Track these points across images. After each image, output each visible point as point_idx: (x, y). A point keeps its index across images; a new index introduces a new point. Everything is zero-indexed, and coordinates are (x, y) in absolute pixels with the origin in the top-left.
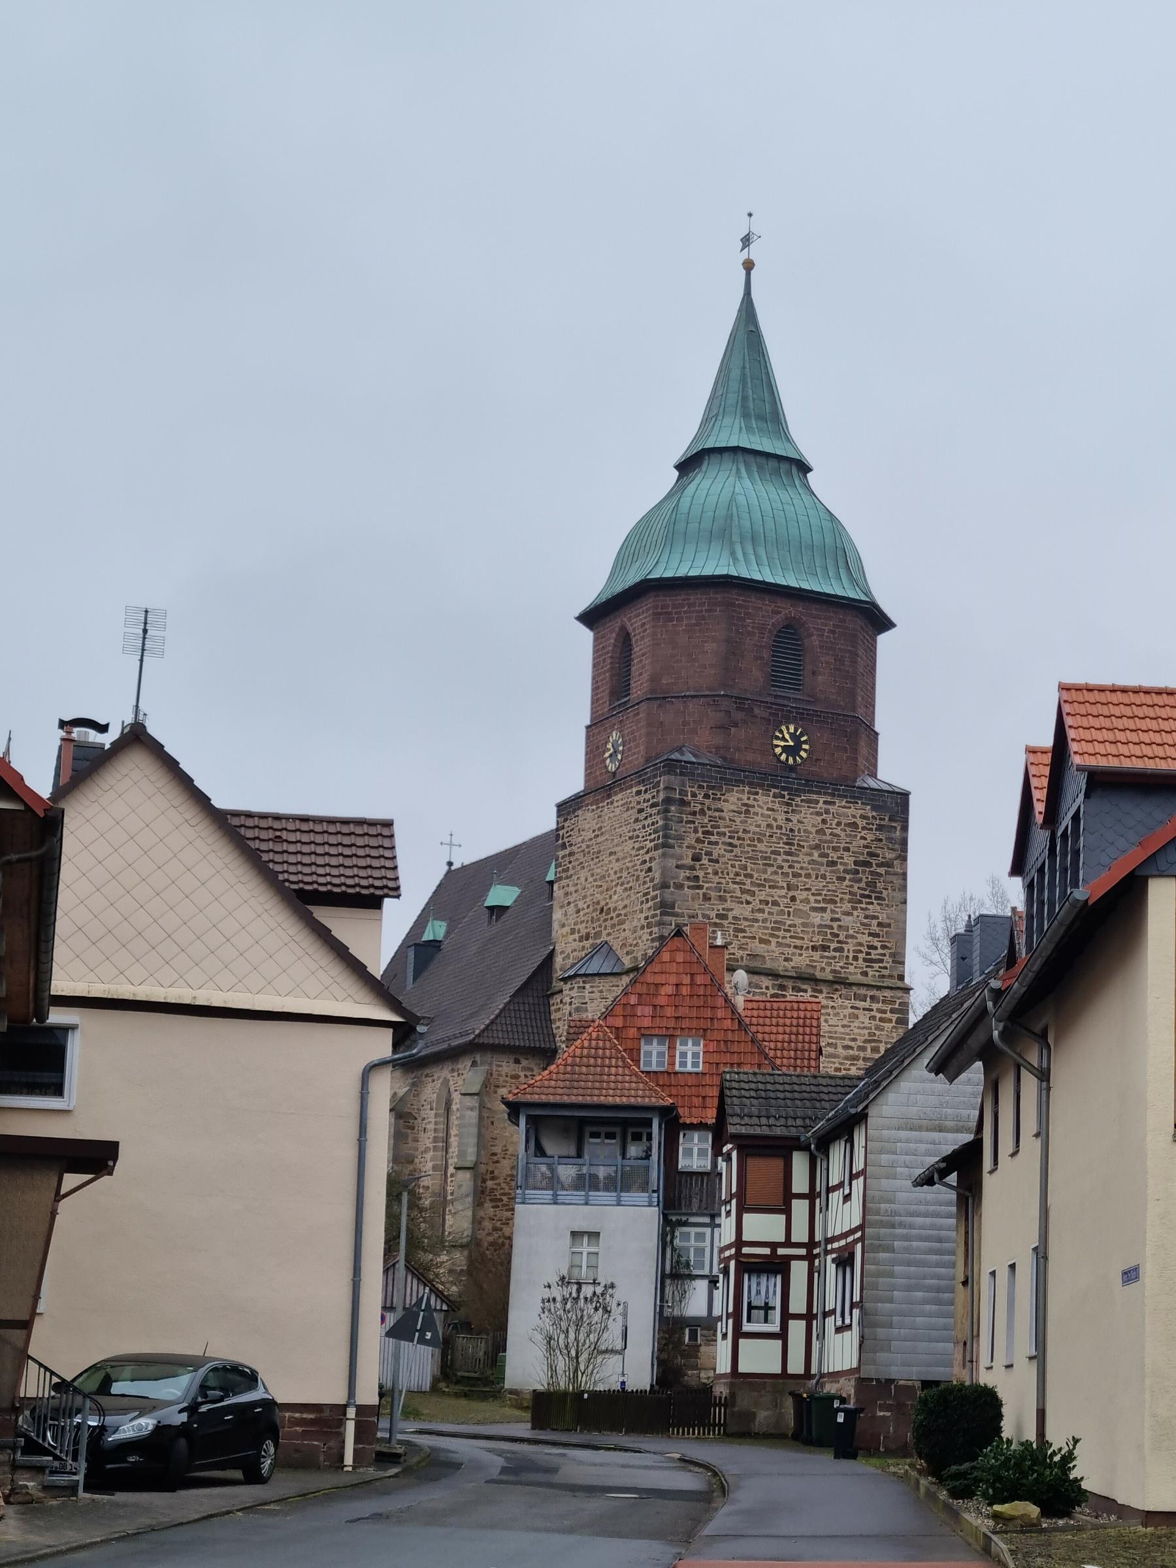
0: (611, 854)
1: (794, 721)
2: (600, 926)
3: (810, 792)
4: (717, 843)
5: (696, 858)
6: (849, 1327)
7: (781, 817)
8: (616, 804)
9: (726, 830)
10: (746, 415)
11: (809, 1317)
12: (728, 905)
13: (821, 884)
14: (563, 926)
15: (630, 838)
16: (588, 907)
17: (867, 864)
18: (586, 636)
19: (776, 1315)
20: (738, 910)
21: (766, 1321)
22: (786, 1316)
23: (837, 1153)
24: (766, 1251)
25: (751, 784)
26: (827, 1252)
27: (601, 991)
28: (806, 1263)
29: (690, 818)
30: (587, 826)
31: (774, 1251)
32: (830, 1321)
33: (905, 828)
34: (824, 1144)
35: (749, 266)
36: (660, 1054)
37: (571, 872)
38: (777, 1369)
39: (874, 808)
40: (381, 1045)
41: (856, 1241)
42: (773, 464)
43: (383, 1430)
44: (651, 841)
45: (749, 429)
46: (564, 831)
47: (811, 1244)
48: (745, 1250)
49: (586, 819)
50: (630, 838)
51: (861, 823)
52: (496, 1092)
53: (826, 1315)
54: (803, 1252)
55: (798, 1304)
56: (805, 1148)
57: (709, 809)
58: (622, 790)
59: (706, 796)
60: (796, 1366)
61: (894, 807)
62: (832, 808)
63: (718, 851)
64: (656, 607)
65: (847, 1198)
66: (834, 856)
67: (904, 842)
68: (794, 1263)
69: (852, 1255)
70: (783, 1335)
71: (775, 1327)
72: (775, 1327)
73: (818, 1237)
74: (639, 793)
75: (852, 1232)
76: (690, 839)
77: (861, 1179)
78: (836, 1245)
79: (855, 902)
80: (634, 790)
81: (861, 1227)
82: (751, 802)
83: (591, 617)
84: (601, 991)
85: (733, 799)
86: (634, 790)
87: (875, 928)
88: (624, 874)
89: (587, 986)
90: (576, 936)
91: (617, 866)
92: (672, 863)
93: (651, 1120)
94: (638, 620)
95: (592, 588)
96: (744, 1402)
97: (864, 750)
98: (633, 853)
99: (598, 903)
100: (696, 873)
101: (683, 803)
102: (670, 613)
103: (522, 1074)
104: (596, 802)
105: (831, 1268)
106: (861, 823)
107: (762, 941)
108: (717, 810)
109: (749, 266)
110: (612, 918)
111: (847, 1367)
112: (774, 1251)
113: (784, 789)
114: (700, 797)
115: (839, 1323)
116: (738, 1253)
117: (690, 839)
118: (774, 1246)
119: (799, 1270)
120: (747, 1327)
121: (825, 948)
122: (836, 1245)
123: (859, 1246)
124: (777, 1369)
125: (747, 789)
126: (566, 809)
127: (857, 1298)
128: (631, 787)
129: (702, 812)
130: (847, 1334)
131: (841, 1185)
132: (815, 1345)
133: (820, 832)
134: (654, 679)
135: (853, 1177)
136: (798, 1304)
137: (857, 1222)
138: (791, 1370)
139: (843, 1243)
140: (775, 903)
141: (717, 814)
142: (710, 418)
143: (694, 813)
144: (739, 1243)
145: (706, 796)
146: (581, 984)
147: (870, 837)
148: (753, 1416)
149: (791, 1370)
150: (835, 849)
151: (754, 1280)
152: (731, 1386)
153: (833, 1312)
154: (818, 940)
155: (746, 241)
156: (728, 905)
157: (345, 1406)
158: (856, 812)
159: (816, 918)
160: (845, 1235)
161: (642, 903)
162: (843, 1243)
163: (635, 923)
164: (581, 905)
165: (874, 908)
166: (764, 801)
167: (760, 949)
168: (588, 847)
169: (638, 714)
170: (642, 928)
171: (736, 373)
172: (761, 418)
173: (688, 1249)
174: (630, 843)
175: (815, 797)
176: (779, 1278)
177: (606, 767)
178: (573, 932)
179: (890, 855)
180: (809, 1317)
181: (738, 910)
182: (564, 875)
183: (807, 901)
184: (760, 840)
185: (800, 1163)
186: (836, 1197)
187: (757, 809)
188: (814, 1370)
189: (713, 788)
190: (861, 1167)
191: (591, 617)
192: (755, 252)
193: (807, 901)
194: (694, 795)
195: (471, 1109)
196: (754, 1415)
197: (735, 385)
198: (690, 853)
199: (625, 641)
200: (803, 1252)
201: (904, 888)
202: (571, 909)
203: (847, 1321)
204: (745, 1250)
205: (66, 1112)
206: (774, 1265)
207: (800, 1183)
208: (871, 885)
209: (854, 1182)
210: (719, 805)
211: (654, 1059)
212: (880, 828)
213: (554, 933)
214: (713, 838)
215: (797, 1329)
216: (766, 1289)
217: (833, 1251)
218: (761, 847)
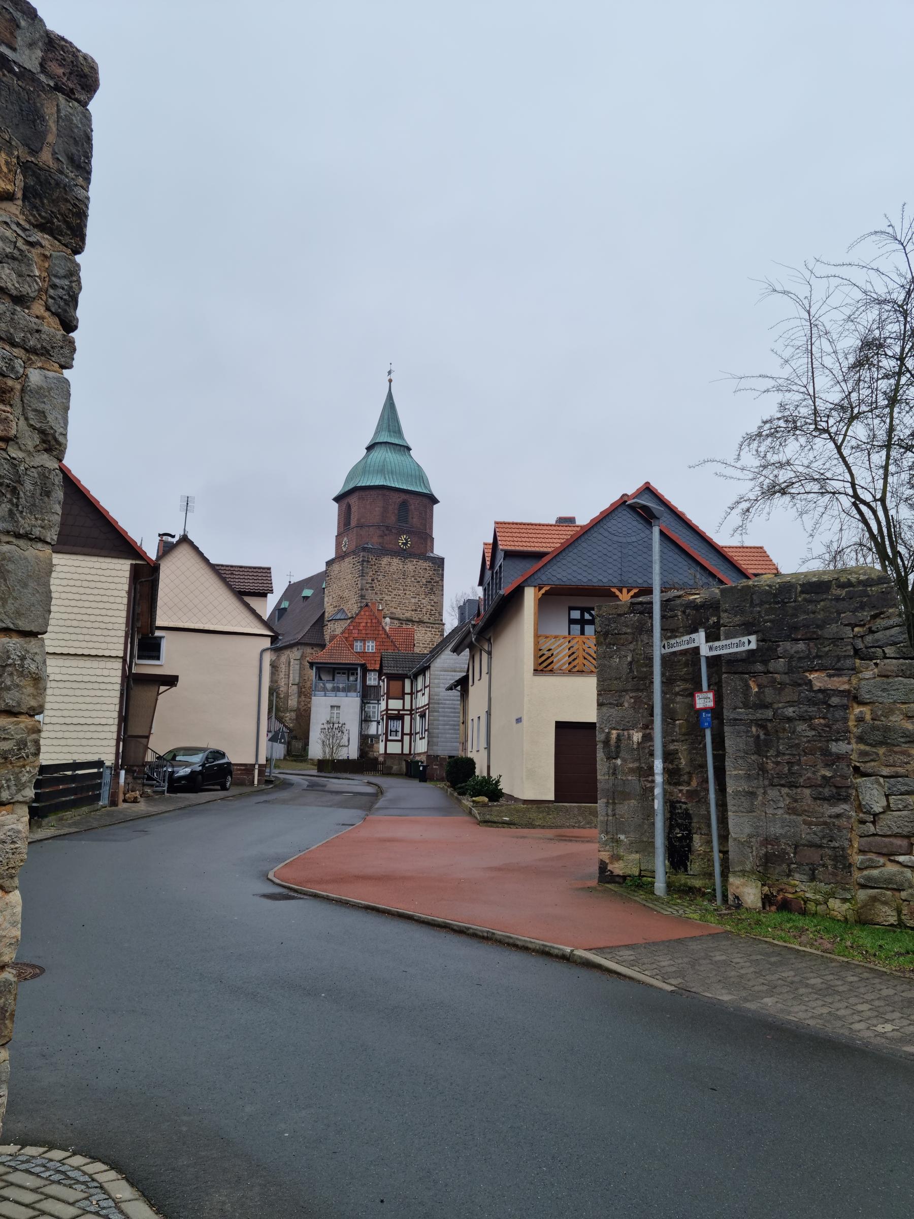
5: (373, 580)
10: (389, 431)
11: (410, 734)
20: (387, 598)
22: (403, 734)
23: (420, 679)
32: (418, 736)
34: (416, 676)
35: (390, 381)
40: (267, 643)
42: (398, 447)
45: (390, 436)
47: (411, 710)
49: (336, 567)
55: (407, 730)
60: (406, 751)
61: (439, 563)
65: (423, 694)
66: (419, 579)
67: (443, 575)
70: (402, 741)
71: (399, 738)
72: (399, 738)
76: (371, 574)
79: (426, 595)
81: (428, 704)
83: (337, 499)
85: (385, 560)
92: (364, 582)
94: (353, 500)
95: (338, 489)
96: (389, 763)
101: (368, 562)
105: (418, 718)
109: (390, 381)
117: (371, 574)
118: (399, 710)
119: (407, 719)
120: (390, 738)
126: (329, 563)
134: (358, 520)
135: (425, 687)
136: (407, 730)
137: (427, 702)
142: (377, 432)
144: (387, 709)
154: (414, 608)
155: (390, 373)
158: (426, 565)
159: (413, 600)
166: (396, 561)
171: (386, 417)
172: (394, 432)
180: (410, 734)
181: (387, 598)
185: (407, 683)
186: (420, 694)
191: (337, 499)
192: (392, 376)
197: (386, 421)
199: (349, 507)
201: (442, 590)
206: (399, 717)
207: (408, 689)
208: (432, 589)
215: (407, 738)
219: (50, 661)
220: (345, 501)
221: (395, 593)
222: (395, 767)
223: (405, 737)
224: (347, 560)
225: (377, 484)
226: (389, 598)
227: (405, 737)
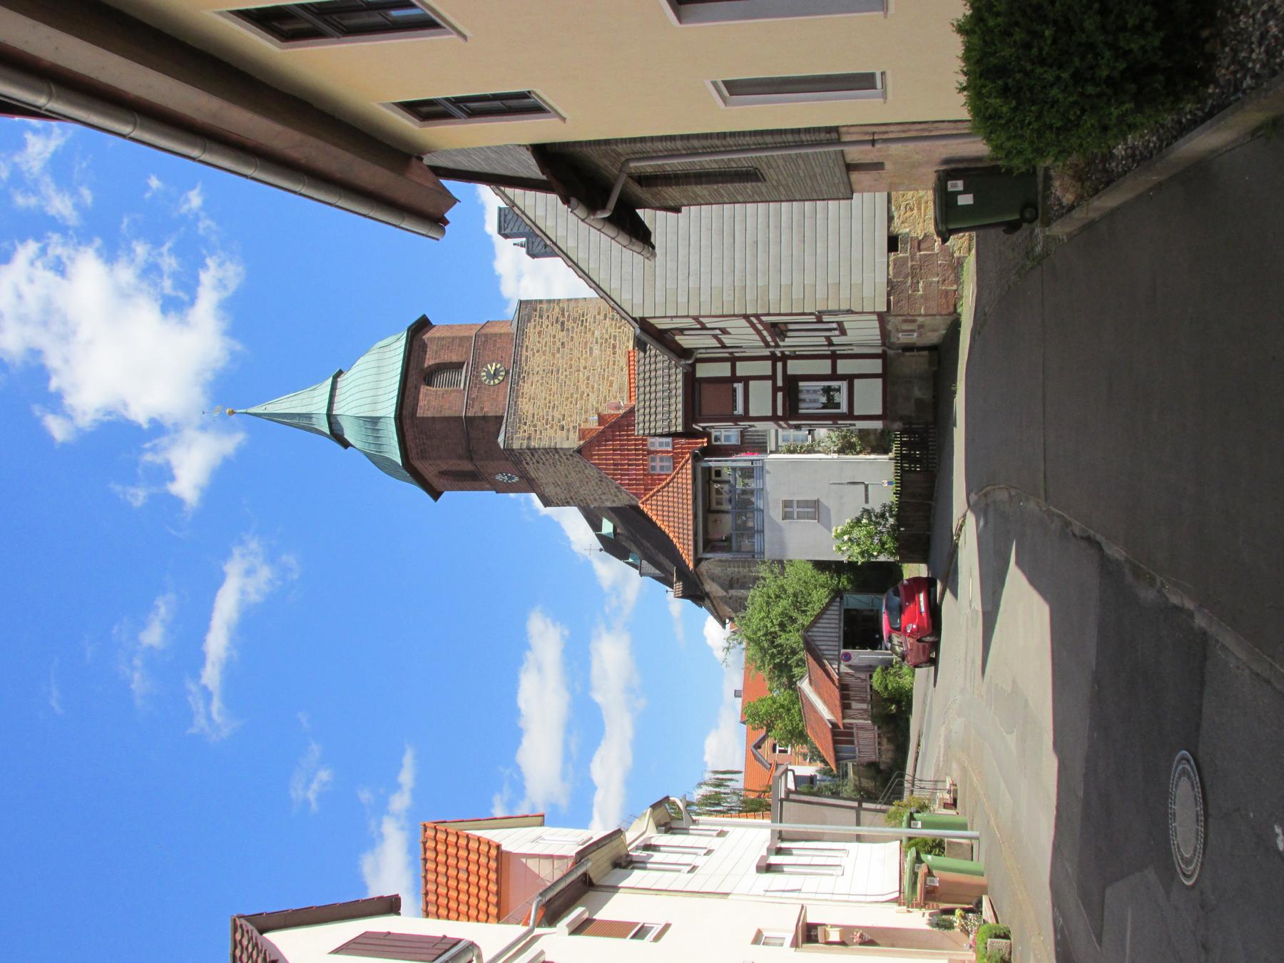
6: (840, 324)
11: (834, 357)
12: (590, 407)
13: (575, 352)
17: (563, 324)
18: (446, 494)
19: (834, 384)
21: (858, 824)
22: (834, 376)
23: (685, 341)
24: (780, 395)
26: (777, 346)
28: (790, 362)
31: (780, 389)
32: (835, 340)
33: (541, 301)
34: (683, 353)
36: (662, 460)
38: (879, 381)
39: (529, 321)
41: (761, 322)
47: (773, 358)
48: (780, 413)
49: (550, 491)
51: (538, 328)
53: (831, 344)
54: (779, 365)
55: (824, 367)
56: (693, 366)
60: (876, 366)
62: (531, 347)
63: (557, 415)
65: (724, 331)
67: (549, 301)
68: (790, 372)
69: (774, 325)
70: (850, 379)
71: (844, 385)
72: (844, 385)
73: (767, 352)
75: (753, 326)
78: (769, 339)
81: (746, 317)
83: (436, 495)
87: (602, 317)
91: (573, 474)
93: (703, 469)
94: (428, 469)
96: (908, 409)
97: (496, 330)
105: (788, 341)
106: (538, 328)
107: (611, 385)
111: (876, 324)
112: (780, 389)
115: (837, 333)
116: (784, 418)
117: (551, 432)
118: (775, 390)
119: (795, 367)
120: (844, 408)
121: (614, 347)
122: (769, 339)
123: (764, 318)
124: (879, 381)
127: (813, 319)
129: (535, 426)
130: (846, 325)
131: (715, 336)
132: (857, 351)
133: (544, 353)
134: (460, 457)
135: (704, 328)
136: (824, 367)
137: (743, 322)
138: (879, 371)
139: (765, 333)
140: (588, 378)
144: (774, 418)
147: (546, 323)
148: (919, 402)
149: (879, 371)
150: (554, 343)
151: (802, 405)
152: (894, 420)
153: (828, 338)
154: (609, 351)
156: (590, 407)
158: (531, 329)
159: (596, 352)
160: (759, 332)
162: (765, 333)
164: (600, 492)
165: (590, 318)
166: (527, 388)
167: (615, 386)
176: (801, 384)
179: (557, 309)
180: (834, 357)
183: (586, 359)
185: (703, 371)
186: (727, 340)
188: (879, 351)
190: (690, 320)
191: (436, 495)
193: (586, 359)
196: (917, 400)
198: (559, 432)
199: (443, 474)
200: (779, 365)
202: (604, 497)
203: (835, 326)
204: (780, 413)
205: (883, 74)
206: (790, 389)
207: (723, 370)
208: (575, 320)
209: (708, 326)
211: (665, 464)
212: (541, 317)
215: (844, 367)
216: (812, 395)
217: (774, 340)
218: (554, 388)
219: (881, 197)
220: (436, 482)
221: (583, 387)
222: (917, 393)
223: (840, 371)
224: (533, 474)
225: (394, 429)
226: (593, 397)
227: (840, 371)
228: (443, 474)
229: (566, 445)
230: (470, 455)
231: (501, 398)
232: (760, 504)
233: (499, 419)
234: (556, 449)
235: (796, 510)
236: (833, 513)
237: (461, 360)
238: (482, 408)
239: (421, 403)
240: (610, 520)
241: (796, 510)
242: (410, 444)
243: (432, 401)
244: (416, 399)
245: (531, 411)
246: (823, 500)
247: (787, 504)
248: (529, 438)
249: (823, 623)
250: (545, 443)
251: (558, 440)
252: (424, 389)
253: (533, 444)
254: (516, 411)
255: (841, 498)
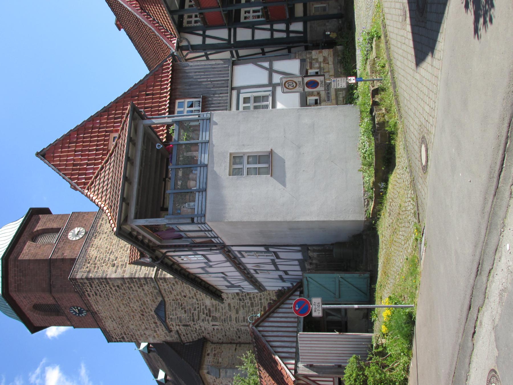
0: (118, 311)
1: (68, 233)
2: (149, 315)
3: (97, 226)
4: (109, 258)
5: (114, 265)
7: (104, 235)
8: (98, 309)
9: (105, 255)
14: (154, 336)
15: (109, 300)
16: (143, 323)
25: (88, 247)
27: (173, 310)
29: (96, 268)
30: (112, 325)
37: (132, 333)
43: (395, 5)
44: (106, 287)
46: (117, 338)
49: (110, 325)
50: (109, 300)
52: (221, 363)
57: (95, 261)
58: (91, 306)
59: (89, 263)
63: (112, 257)
64: (15, 291)
74: (90, 296)
77: (274, 268)
80: (89, 298)
82: (95, 247)
84: (173, 310)
86: (89, 298)
88: (125, 302)
89: (171, 317)
90: (157, 329)
91: (123, 307)
94: (25, 303)
98: (114, 297)
99: (140, 317)
100: (120, 265)
102: (18, 284)
103: (214, 352)
104: (101, 320)
108: (96, 259)
110: (144, 309)
113: (93, 235)
114: (89, 265)
117: (105, 268)
125: (90, 248)
128: (88, 300)
141: (97, 259)
143: (95, 267)
145: (89, 263)
146: (170, 320)
157: (355, 75)
161: (133, 290)
163: (142, 294)
164: (143, 328)
166: (97, 242)
168: (119, 325)
169: (59, 298)
170: (143, 290)
173: (241, 163)
174: (111, 299)
175: (99, 225)
177: (86, 315)
178: (155, 331)
182: (134, 337)
184: (112, 242)
187: (99, 244)
189: (86, 260)
194: (87, 267)
195: (226, 372)
199: (37, 307)
210: (94, 257)
213: (159, 342)
214: (107, 259)
220: (35, 317)
228: (37, 307)
229: (114, 276)
230: (50, 289)
231: (77, 248)
232: (204, 159)
233: (73, 261)
234: (106, 279)
235: (246, 166)
236: (288, 164)
237: (59, 227)
238: (63, 254)
239: (24, 251)
240: (164, 370)
241: (246, 166)
242: (11, 279)
243: (30, 251)
244: (22, 249)
245: (95, 255)
246: (278, 151)
247: (236, 159)
248: (89, 272)
249: (277, 317)
250: (100, 275)
251: (109, 273)
252: (29, 243)
253: (91, 275)
254: (85, 255)
255: (299, 147)
